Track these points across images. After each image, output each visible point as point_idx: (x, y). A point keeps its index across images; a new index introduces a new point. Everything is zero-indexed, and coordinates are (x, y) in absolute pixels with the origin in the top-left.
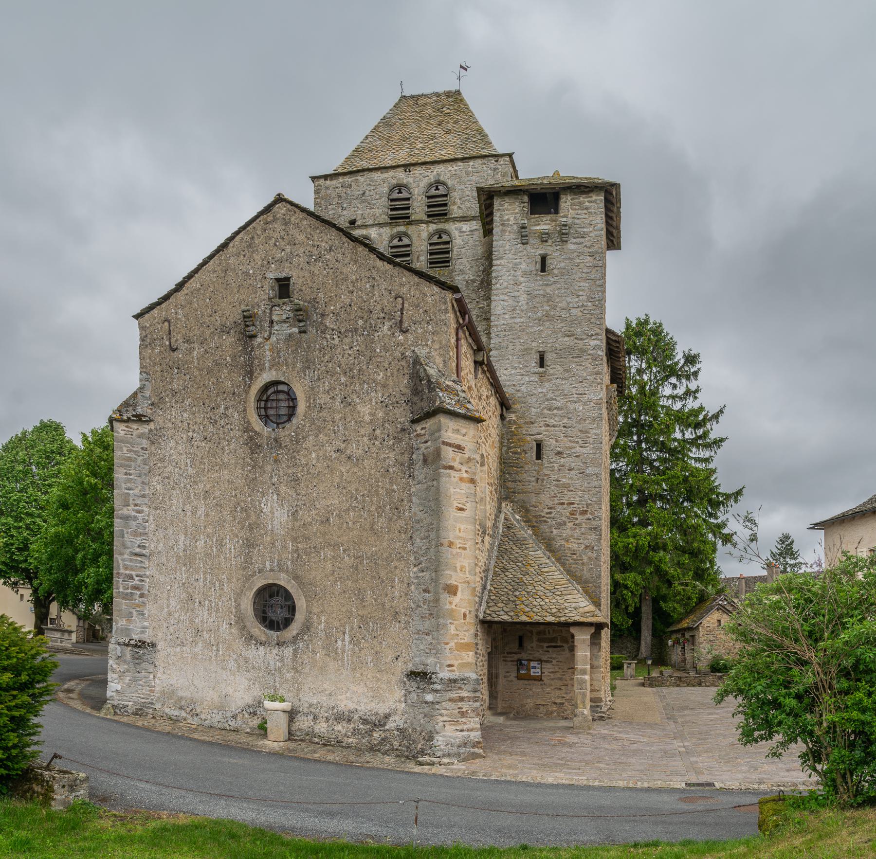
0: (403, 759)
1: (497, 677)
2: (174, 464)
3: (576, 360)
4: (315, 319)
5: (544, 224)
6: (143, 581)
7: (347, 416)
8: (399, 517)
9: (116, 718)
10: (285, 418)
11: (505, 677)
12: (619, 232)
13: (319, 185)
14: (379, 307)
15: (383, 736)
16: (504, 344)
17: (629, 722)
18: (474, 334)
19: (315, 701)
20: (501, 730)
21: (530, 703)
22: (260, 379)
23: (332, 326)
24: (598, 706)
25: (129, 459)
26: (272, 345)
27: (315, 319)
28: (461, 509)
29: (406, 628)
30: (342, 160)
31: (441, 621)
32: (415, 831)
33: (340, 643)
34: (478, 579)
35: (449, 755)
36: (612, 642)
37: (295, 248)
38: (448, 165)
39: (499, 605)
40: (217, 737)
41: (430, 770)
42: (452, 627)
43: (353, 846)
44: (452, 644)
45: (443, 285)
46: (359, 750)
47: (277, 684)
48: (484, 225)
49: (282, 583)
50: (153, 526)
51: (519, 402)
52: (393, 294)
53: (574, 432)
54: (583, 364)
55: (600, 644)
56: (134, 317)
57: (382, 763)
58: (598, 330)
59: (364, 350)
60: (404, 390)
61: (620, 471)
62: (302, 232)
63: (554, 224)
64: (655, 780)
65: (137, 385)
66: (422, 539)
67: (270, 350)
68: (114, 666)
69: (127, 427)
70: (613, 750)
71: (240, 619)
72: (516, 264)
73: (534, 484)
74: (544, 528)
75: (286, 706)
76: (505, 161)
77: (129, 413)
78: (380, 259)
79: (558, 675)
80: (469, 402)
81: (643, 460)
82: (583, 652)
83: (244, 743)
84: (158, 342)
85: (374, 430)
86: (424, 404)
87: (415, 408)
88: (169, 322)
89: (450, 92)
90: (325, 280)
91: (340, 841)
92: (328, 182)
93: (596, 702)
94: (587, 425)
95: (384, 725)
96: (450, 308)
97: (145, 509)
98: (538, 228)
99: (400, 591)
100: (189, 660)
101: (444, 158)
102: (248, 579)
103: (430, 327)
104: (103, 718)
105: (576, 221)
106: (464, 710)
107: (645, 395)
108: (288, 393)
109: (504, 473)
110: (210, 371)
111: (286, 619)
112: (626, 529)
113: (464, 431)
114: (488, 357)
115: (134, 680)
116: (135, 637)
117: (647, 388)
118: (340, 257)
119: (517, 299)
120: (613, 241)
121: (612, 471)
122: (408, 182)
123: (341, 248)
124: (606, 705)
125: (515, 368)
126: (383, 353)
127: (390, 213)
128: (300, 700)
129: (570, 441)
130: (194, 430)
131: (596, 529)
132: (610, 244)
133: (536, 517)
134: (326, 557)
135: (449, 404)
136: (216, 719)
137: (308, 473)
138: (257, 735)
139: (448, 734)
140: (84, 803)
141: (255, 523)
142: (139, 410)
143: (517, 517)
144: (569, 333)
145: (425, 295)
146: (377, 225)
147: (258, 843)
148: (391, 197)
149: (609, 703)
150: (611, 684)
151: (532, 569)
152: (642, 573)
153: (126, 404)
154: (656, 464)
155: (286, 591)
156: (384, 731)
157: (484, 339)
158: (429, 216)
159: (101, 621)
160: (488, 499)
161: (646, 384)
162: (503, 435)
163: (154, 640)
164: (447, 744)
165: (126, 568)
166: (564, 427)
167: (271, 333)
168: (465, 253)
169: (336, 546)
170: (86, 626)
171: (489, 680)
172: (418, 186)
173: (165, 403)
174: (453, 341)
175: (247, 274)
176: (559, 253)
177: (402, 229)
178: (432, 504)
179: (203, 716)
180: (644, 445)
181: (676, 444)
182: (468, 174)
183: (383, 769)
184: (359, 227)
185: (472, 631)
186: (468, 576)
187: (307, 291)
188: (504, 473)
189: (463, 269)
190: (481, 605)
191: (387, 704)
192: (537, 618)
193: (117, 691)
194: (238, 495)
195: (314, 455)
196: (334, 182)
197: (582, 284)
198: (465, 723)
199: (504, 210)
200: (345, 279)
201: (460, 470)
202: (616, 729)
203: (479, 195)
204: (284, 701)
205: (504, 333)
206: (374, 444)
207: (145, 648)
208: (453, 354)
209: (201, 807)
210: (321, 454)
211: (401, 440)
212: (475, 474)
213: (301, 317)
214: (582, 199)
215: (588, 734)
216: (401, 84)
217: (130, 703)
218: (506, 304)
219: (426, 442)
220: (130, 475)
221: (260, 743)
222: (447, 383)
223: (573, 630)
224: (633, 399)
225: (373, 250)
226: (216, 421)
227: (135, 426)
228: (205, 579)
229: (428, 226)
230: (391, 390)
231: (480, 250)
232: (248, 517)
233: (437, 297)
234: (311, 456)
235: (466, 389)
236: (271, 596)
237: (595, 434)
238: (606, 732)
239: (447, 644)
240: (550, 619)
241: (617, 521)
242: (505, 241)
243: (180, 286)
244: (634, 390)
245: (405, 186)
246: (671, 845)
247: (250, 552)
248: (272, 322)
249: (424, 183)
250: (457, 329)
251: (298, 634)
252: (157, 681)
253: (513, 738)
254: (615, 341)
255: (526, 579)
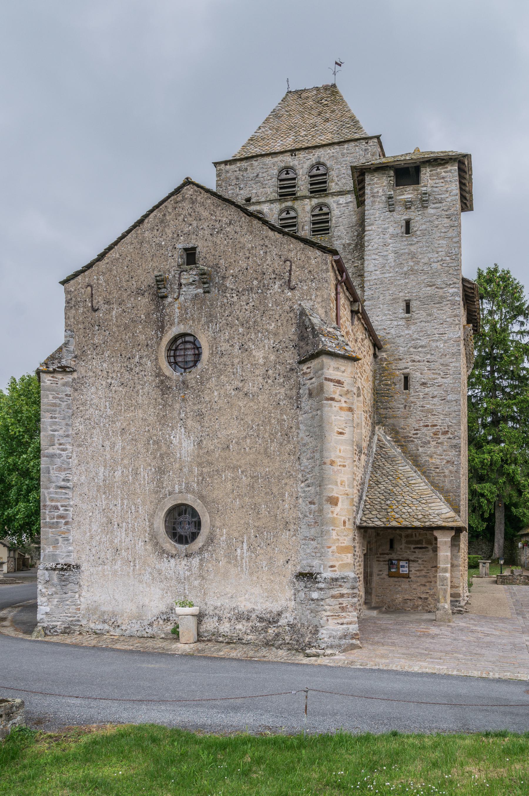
0: (294, 652)
1: (371, 575)
2: (94, 407)
3: (437, 305)
4: (217, 281)
5: (408, 194)
6: (67, 510)
7: (246, 360)
8: (289, 442)
9: (47, 639)
10: (191, 364)
11: (378, 575)
12: (471, 196)
13: (220, 170)
14: (270, 270)
15: (276, 631)
16: (376, 295)
17: (484, 616)
18: (350, 289)
19: (219, 604)
20: (375, 623)
21: (399, 598)
22: (170, 332)
23: (231, 287)
24: (457, 601)
25: (54, 405)
26: (180, 303)
27: (217, 281)
28: (341, 433)
29: (295, 535)
30: (239, 148)
31: (324, 527)
32: (305, 719)
33: (239, 551)
34: (356, 491)
35: (332, 647)
36: (470, 543)
37: (200, 223)
38: (327, 148)
39: (373, 513)
40: (136, 645)
41: (316, 661)
42: (334, 533)
43: (254, 739)
44: (334, 548)
45: (324, 249)
46: (257, 645)
47: (186, 591)
48: (357, 198)
49: (189, 503)
50: (76, 462)
51: (389, 343)
52: (283, 259)
53: (437, 365)
54: (443, 308)
55: (459, 545)
56: (60, 283)
57: (276, 656)
58: (455, 280)
59: (258, 305)
60: (292, 337)
61: (476, 397)
62: (206, 209)
63: (416, 193)
64: (505, 671)
65: (62, 341)
66: (308, 459)
67: (179, 308)
68: (43, 590)
69: (52, 377)
70: (469, 642)
71: (154, 536)
72: (385, 229)
73: (403, 410)
74: (411, 446)
75: (195, 610)
76: (374, 142)
77: (56, 365)
78: (272, 230)
79: (423, 573)
80: (347, 345)
81: (495, 387)
82: (444, 553)
83: (160, 648)
84: (81, 304)
85: (267, 371)
86: (310, 348)
87: (302, 351)
88: (91, 287)
89: (327, 86)
90: (226, 249)
91: (244, 735)
92: (228, 167)
93: (455, 596)
94: (447, 359)
95: (277, 621)
96: (330, 268)
97: (68, 447)
98: (403, 197)
99: (289, 504)
100: (110, 576)
101: (324, 143)
102: (160, 501)
103: (314, 284)
104: (34, 641)
105: (435, 189)
106: (344, 605)
107: (496, 332)
108: (194, 343)
109: (377, 402)
110: (126, 327)
111: (193, 533)
112: (482, 447)
113: (343, 368)
114: (363, 307)
115: (62, 601)
116: (62, 561)
117: (498, 326)
118: (238, 229)
119: (386, 258)
120: (466, 203)
121: (469, 397)
122: (294, 165)
123: (239, 222)
124: (464, 600)
125: (385, 315)
126: (275, 307)
127: (279, 191)
128: (206, 604)
129: (433, 373)
130: (112, 378)
131: (456, 447)
132: (464, 206)
133: (404, 437)
134: (226, 478)
135: (330, 347)
136: (135, 628)
137: (211, 409)
138: (170, 639)
139: (331, 627)
140: (21, 730)
141: (166, 453)
142: (64, 363)
143: (388, 438)
144: (431, 284)
145: (309, 258)
146: (268, 201)
147: (176, 744)
148: (280, 178)
149: (466, 598)
150: (469, 581)
151: (401, 482)
152: (495, 483)
153: (52, 358)
154: (508, 390)
155: (193, 509)
156: (277, 627)
157: (359, 292)
158: (312, 192)
159: (30, 550)
160: (364, 423)
161: (497, 323)
162: (375, 370)
163: (79, 562)
164: (330, 637)
165: (52, 500)
166: (428, 362)
167: (179, 294)
168: (342, 222)
169: (235, 468)
170: (17, 556)
171: (364, 578)
172: (302, 168)
173: (87, 356)
174: (333, 295)
175: (159, 245)
176: (420, 217)
177: (289, 204)
178: (317, 429)
179: (124, 627)
180: (496, 374)
181: (525, 372)
182: (343, 155)
183: (277, 662)
184: (254, 204)
185: (351, 536)
186: (347, 489)
187: (210, 258)
188: (377, 402)
189: (341, 235)
190: (358, 513)
191: (280, 602)
192: (405, 523)
193: (47, 613)
194: (151, 430)
195: (216, 393)
196: (233, 167)
197: (440, 242)
198: (345, 617)
199: (374, 184)
200: (242, 248)
201: (340, 401)
202: (472, 622)
203: (353, 173)
204: (193, 605)
205: (376, 286)
206: (267, 382)
207: (70, 570)
208: (333, 305)
209: (125, 715)
210: (222, 392)
211: (289, 379)
212: (352, 404)
213: (205, 280)
214: (439, 170)
215: (448, 626)
216: (288, 81)
217: (59, 623)
218: (377, 262)
219: (311, 379)
220: (55, 418)
221: (174, 646)
222: (328, 329)
223: (436, 533)
224: (485, 336)
225: (265, 222)
226: (131, 369)
227: (60, 376)
228: (123, 504)
229: (311, 201)
230: (281, 338)
231: (354, 219)
232: (160, 448)
233: (319, 259)
234: (214, 394)
235: (344, 334)
236: (180, 515)
237: (455, 367)
238: (464, 624)
239: (330, 547)
240: (417, 524)
241: (473, 439)
242: (375, 210)
243: (101, 257)
244: (487, 328)
245: (292, 168)
246: (517, 736)
247: (161, 477)
248: (180, 285)
249: (307, 165)
250: (336, 285)
251: (203, 546)
252: (82, 599)
253: (385, 630)
254: (471, 288)
255: (396, 490)
